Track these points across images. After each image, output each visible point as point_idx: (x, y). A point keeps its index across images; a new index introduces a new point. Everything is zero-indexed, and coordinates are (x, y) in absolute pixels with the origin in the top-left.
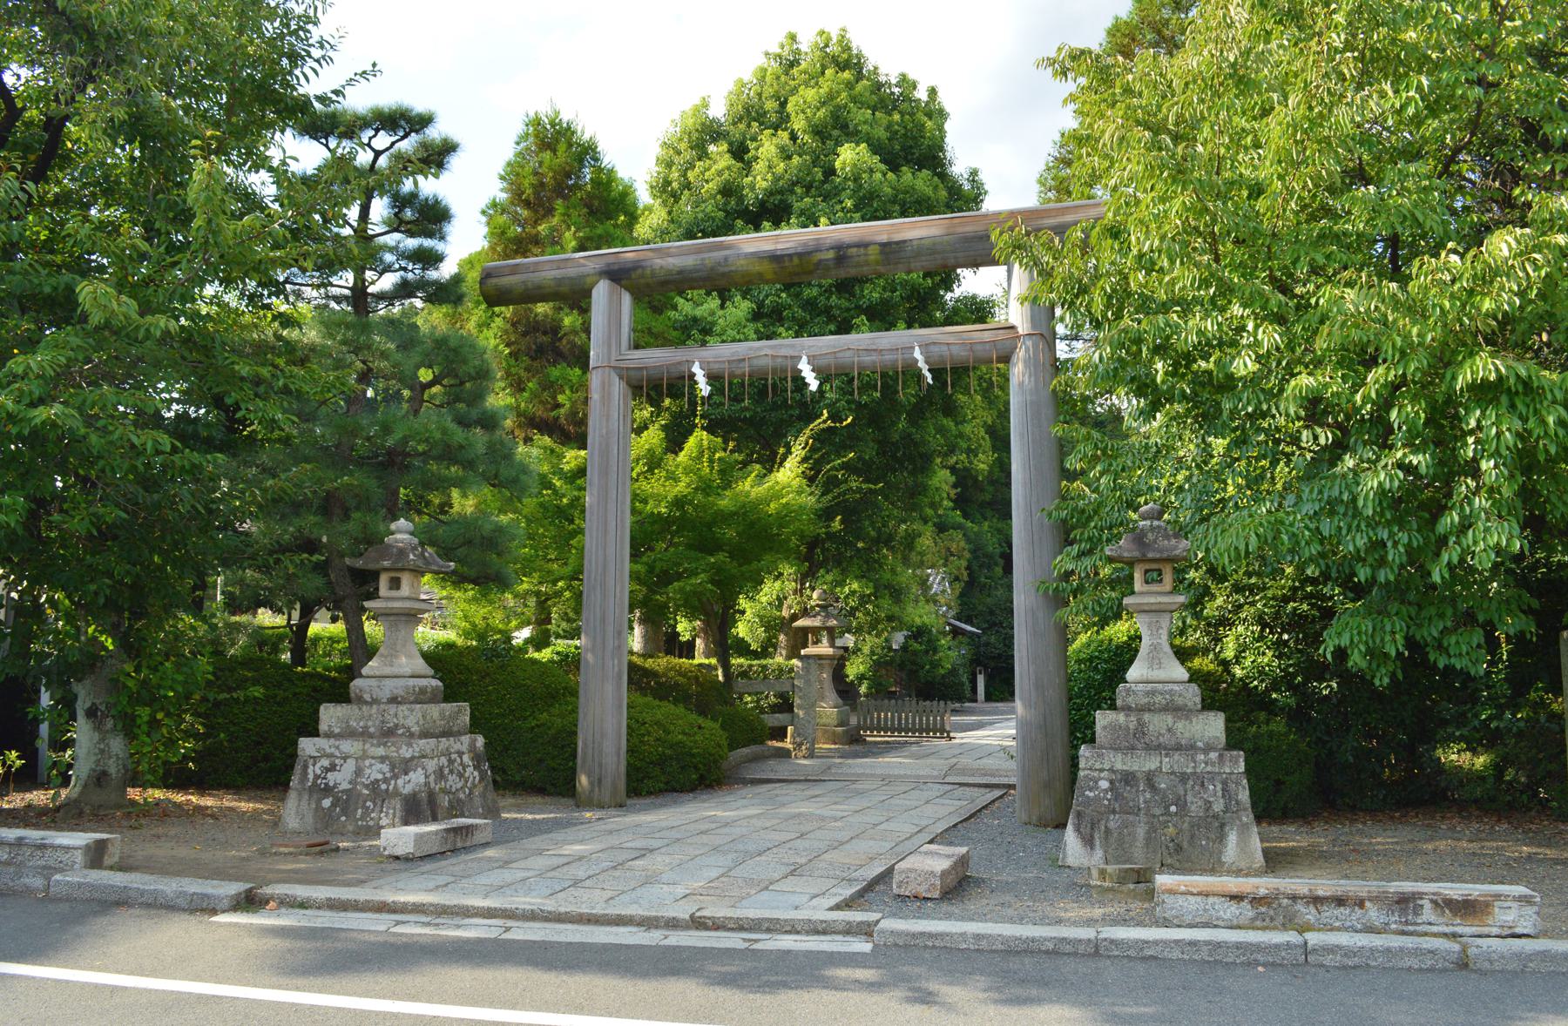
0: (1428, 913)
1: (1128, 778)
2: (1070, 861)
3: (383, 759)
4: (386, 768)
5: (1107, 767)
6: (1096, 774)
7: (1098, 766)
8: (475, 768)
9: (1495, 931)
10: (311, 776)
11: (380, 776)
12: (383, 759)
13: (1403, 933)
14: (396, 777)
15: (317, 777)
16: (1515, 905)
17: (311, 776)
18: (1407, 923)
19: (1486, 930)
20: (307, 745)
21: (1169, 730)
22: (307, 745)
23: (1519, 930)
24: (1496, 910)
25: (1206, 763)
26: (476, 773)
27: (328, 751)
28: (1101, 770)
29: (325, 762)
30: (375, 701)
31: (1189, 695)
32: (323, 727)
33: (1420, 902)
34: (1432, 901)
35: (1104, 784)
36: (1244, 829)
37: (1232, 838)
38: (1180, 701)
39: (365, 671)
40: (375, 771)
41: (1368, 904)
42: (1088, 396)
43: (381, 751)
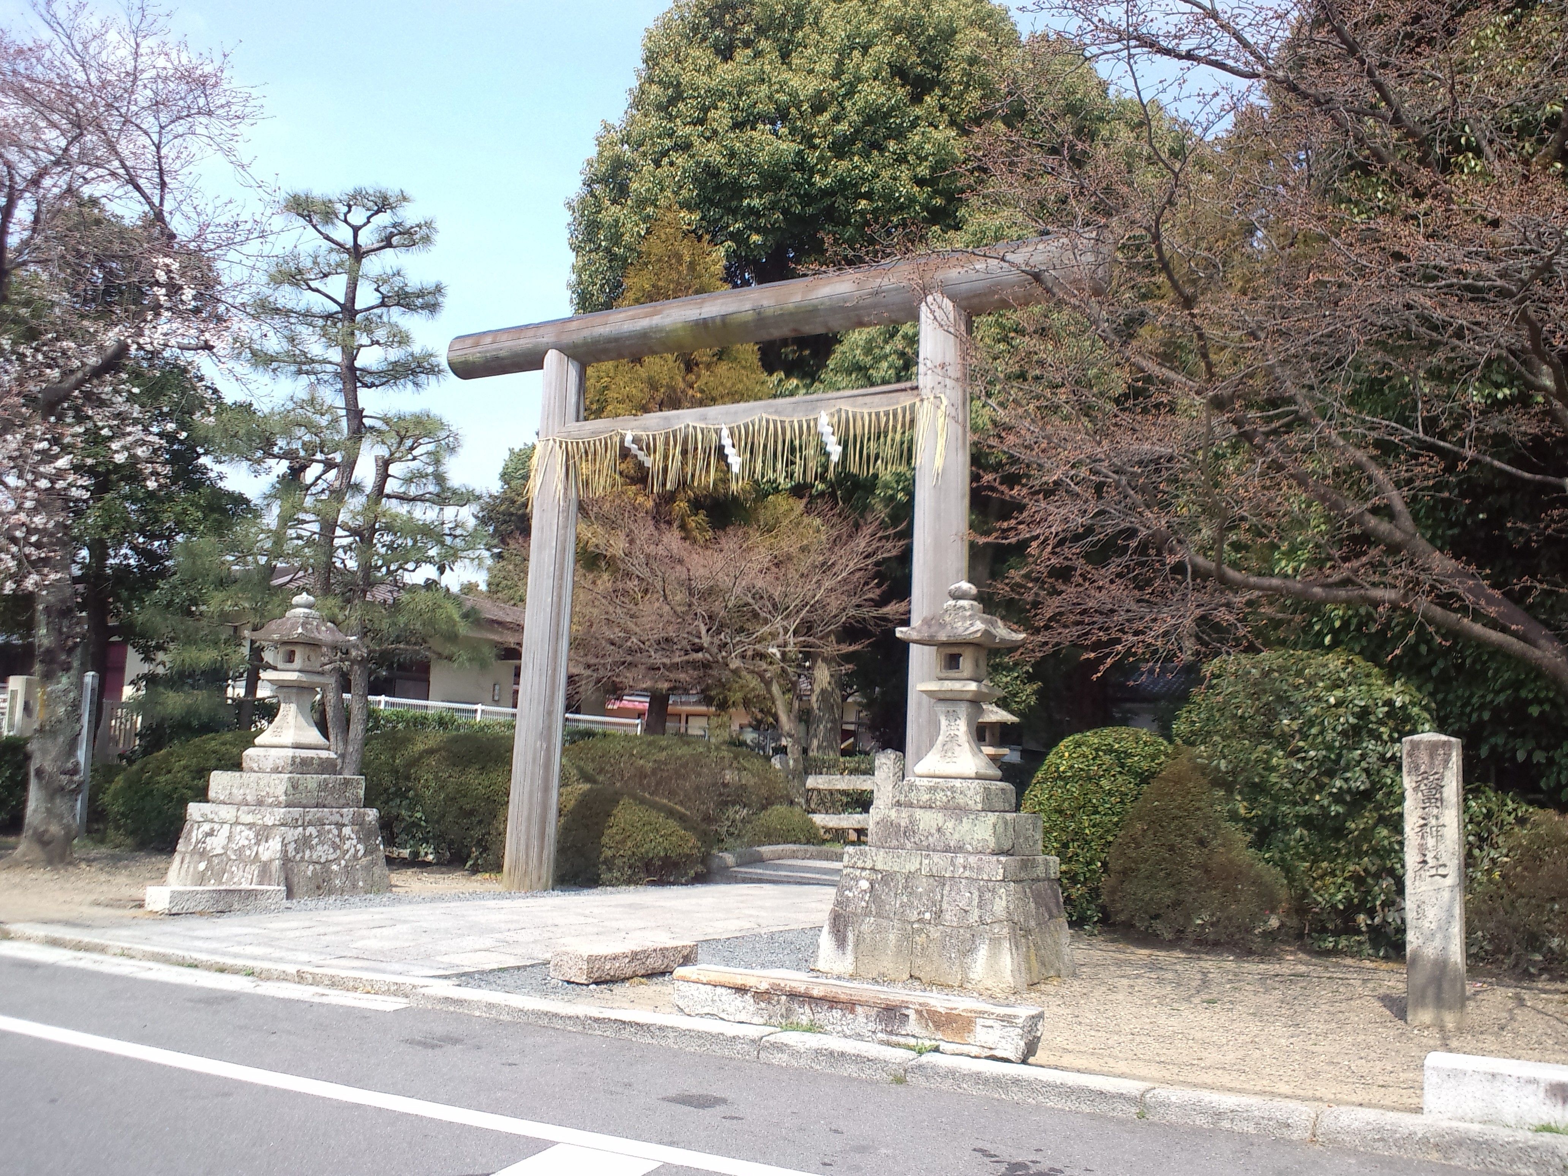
0: (913, 1025)
1: (887, 878)
2: (821, 965)
3: (251, 826)
4: (252, 835)
5: (869, 865)
6: (858, 872)
7: (860, 864)
8: (359, 840)
9: (975, 1051)
10: (194, 840)
11: (246, 843)
12: (251, 826)
13: (888, 1044)
14: (258, 843)
15: (197, 842)
16: (997, 1025)
17: (194, 840)
18: (891, 1033)
19: (965, 1049)
20: (194, 810)
21: (939, 830)
22: (194, 810)
23: (998, 1053)
24: (978, 1028)
25: (965, 867)
26: (360, 847)
27: (210, 816)
28: (863, 869)
29: (206, 827)
30: (261, 771)
31: (970, 793)
32: (211, 794)
33: (906, 1012)
34: (917, 1011)
35: (864, 885)
36: (995, 942)
37: (983, 952)
38: (961, 800)
39: (257, 741)
40: (243, 837)
41: (859, 1009)
42: (105, 316)
43: (249, 819)
